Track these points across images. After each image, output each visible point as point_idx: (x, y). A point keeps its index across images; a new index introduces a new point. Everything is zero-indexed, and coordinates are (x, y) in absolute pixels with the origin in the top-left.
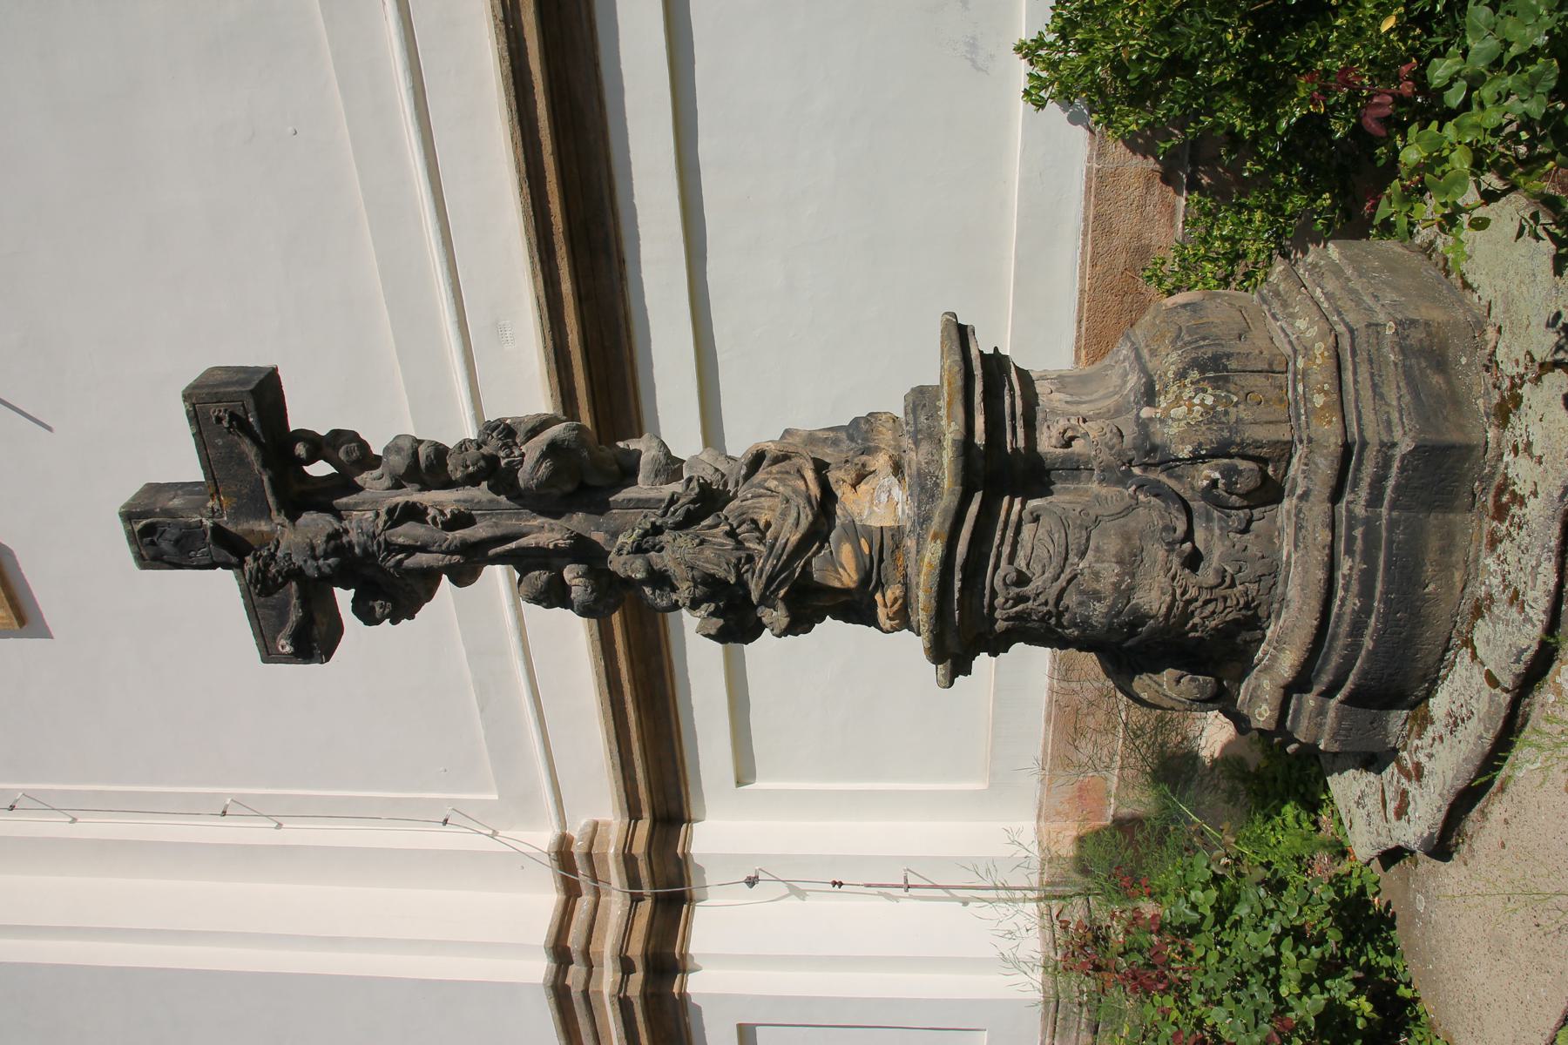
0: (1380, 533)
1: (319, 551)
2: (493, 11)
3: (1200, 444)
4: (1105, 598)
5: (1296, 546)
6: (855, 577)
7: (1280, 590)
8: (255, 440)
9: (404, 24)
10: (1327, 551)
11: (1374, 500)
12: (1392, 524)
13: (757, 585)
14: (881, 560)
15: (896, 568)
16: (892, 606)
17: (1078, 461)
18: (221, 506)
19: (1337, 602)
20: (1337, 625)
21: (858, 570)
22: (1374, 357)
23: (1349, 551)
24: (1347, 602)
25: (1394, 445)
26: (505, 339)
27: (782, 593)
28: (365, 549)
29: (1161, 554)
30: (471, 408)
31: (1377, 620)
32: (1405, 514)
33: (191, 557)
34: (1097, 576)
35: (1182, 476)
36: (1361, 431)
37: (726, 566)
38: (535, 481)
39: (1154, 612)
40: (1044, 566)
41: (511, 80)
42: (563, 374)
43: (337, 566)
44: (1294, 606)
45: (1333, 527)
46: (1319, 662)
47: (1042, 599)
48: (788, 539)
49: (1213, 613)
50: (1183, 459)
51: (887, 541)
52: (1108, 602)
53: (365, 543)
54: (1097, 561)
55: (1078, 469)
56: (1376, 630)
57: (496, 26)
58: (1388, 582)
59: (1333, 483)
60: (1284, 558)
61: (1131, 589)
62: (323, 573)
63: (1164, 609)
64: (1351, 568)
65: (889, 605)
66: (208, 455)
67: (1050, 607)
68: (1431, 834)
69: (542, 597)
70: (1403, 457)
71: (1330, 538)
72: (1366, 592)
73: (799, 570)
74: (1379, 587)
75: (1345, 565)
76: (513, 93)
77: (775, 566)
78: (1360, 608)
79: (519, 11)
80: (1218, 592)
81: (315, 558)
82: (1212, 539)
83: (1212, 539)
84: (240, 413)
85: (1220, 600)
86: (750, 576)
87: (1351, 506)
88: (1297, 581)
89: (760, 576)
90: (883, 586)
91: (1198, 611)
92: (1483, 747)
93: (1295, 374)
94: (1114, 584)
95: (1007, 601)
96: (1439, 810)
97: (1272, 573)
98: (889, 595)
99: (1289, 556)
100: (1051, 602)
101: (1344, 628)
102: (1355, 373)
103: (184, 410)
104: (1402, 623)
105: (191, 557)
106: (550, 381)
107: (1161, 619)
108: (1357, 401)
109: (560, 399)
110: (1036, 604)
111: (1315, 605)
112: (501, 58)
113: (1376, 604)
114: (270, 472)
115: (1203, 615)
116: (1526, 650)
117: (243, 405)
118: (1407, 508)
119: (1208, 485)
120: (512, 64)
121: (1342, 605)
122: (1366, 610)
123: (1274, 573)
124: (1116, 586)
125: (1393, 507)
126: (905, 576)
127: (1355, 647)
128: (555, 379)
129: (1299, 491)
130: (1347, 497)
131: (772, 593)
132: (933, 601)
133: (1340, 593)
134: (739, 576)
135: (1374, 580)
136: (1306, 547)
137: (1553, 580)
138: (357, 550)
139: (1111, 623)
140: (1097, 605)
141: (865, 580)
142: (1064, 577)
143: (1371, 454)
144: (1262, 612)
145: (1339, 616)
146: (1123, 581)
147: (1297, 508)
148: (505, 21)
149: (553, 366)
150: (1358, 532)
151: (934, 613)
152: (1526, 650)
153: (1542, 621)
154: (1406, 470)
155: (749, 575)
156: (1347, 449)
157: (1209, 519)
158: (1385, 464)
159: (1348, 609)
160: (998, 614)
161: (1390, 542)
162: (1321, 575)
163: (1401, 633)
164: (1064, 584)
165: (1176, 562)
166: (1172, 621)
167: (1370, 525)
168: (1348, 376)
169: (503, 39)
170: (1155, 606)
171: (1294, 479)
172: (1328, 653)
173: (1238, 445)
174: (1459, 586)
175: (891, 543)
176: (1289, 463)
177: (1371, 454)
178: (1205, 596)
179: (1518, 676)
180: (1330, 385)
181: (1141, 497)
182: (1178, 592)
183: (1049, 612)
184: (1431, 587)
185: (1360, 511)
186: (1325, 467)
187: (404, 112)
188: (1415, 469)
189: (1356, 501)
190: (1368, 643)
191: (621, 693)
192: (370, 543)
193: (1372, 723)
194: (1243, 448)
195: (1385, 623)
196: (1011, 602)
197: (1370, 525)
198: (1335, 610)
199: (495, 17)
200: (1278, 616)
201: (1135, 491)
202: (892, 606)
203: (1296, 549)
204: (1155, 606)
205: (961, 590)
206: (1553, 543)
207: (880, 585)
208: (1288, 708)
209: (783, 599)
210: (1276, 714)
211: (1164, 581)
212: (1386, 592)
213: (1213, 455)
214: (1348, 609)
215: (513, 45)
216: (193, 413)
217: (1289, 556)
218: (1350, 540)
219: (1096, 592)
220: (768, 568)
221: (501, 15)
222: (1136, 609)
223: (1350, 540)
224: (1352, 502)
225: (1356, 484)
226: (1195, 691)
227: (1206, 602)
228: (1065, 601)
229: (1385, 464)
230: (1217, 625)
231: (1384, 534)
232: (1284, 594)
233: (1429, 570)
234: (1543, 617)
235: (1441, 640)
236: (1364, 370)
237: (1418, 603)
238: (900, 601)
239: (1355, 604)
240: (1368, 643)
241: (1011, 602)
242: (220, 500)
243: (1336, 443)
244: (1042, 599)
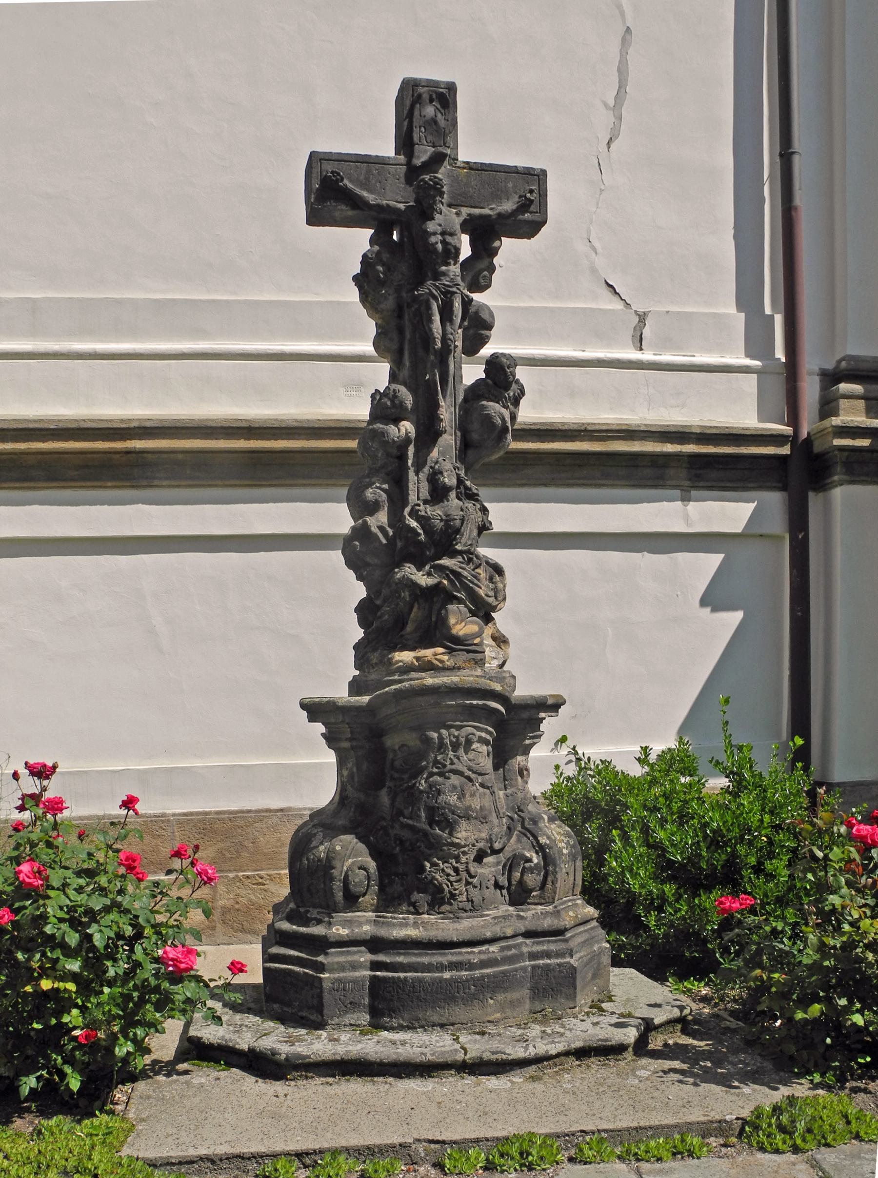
0: (517, 963)
1: (449, 239)
2: (592, 424)
3: (551, 848)
4: (461, 802)
5: (495, 918)
6: (461, 633)
7: (465, 915)
8: (514, 213)
9: (573, 362)
10: (502, 935)
11: (533, 956)
12: (524, 969)
13: (455, 565)
14: (468, 651)
15: (465, 662)
16: (436, 659)
17: (511, 779)
18: (459, 167)
19: (469, 950)
20: (452, 954)
21: (466, 635)
22: (594, 940)
23: (503, 949)
24: (474, 954)
25: (572, 956)
26: (349, 389)
27: (445, 582)
28: (444, 274)
29: (484, 835)
30: (291, 351)
31: (467, 975)
32: (529, 975)
33: (420, 127)
34: (473, 795)
35: (521, 843)
36: (572, 937)
37: (469, 543)
38: (494, 414)
39: (455, 835)
40: (474, 760)
41: (549, 428)
42: (335, 432)
43: (436, 249)
44: (457, 926)
45: (514, 936)
46: (416, 951)
47: (455, 760)
48: (481, 588)
49: (448, 875)
50: (538, 841)
51: (479, 656)
52: (459, 804)
53: (448, 276)
54: (480, 794)
55: (505, 780)
56: (460, 977)
57: (583, 424)
58: (495, 975)
59: (539, 929)
60: (485, 913)
61: (468, 818)
62: (430, 237)
63: (457, 841)
64: (493, 952)
65: (438, 657)
66: (500, 172)
67: (449, 767)
68: (309, 1057)
69: (397, 402)
70: (569, 963)
71: (509, 935)
72: (483, 964)
73: (459, 595)
74: (489, 971)
75: (494, 948)
76: (542, 428)
77: (466, 578)
78: (474, 963)
79: (590, 440)
80: (464, 875)
81: (443, 233)
82: (490, 869)
83: (490, 869)
84: (532, 208)
85: (458, 878)
86: (459, 560)
87: (524, 945)
88: (475, 923)
89: (461, 568)
90: (449, 653)
91: (450, 865)
92: (417, 1057)
93: (574, 900)
94: (471, 806)
95: (454, 737)
96: (334, 1054)
97: (473, 908)
98: (445, 658)
99: (487, 915)
100: (453, 767)
101: (454, 959)
102: (585, 931)
103: (535, 167)
104: (467, 991)
105: (420, 127)
106: (331, 420)
107: (449, 840)
108: (576, 935)
109: (316, 426)
110: (452, 757)
111: (467, 936)
112: (564, 424)
113: (477, 972)
114: (494, 217)
115: (445, 869)
116: (505, 1054)
117: (537, 212)
118: (533, 976)
119: (526, 857)
120: (560, 430)
121: (468, 953)
122: (471, 966)
123: (474, 909)
124: (469, 808)
125: (534, 967)
126: (459, 668)
127: (441, 968)
128: (333, 425)
129: (522, 914)
130: (528, 941)
131: (447, 575)
132: (469, 685)
133: (476, 950)
134: (460, 553)
135: (492, 967)
136: (496, 924)
137: (553, 1052)
138: (444, 268)
139: (444, 808)
140: (455, 797)
141: (457, 640)
142: (473, 776)
143: (561, 946)
144: (446, 908)
145: (460, 953)
146: (473, 812)
147: (511, 916)
148: (586, 430)
149: (344, 425)
150: (513, 951)
151: (460, 686)
152: (505, 1054)
153: (530, 1055)
154: (560, 967)
155: (461, 559)
156: (558, 933)
157: (498, 863)
158: (559, 954)
159: (471, 957)
160: (444, 732)
161: (516, 970)
162: (488, 935)
163: (458, 992)
164: (466, 774)
165: (481, 845)
166: (445, 848)
167: (519, 957)
168: (582, 929)
169: (576, 427)
170: (459, 835)
171: (529, 910)
172: (428, 954)
173: (555, 870)
174: (491, 1018)
175: (479, 658)
176: (541, 904)
177: (561, 946)
178: (461, 867)
179: (481, 1058)
180: (581, 918)
181: (504, 820)
182: (466, 849)
183: (445, 766)
184: (491, 1002)
185: (525, 950)
186: (547, 923)
187: (515, 348)
188: (560, 972)
189: (529, 946)
190: (447, 975)
191: (15, 440)
192: (448, 279)
193: (351, 1003)
194: (553, 873)
195: (467, 981)
196: (454, 740)
197: (519, 957)
198: (464, 950)
199: (588, 424)
200: (443, 919)
201: (508, 816)
202: (436, 659)
203: (493, 918)
204: (459, 835)
205: (472, 705)
206: (573, 1046)
207: (450, 651)
208: (348, 947)
209: (440, 583)
210: (347, 939)
211: (472, 839)
212: (488, 976)
213: (545, 857)
214: (471, 957)
215: (570, 433)
216: (532, 172)
217: (487, 915)
218: (509, 948)
219: (464, 795)
220: (465, 573)
221: (589, 428)
222: (456, 822)
223: (509, 948)
224: (526, 944)
225: (538, 943)
226: (357, 880)
227: (456, 870)
228: (453, 777)
229: (559, 954)
230: (437, 880)
231: (517, 966)
232: (462, 918)
233: (500, 997)
234: (533, 1054)
235: (452, 1020)
236: (585, 936)
237: (481, 997)
238: (440, 665)
239: (474, 959)
240: (447, 975)
241: (454, 740)
242: (464, 168)
243: (566, 925)
244: (455, 760)
